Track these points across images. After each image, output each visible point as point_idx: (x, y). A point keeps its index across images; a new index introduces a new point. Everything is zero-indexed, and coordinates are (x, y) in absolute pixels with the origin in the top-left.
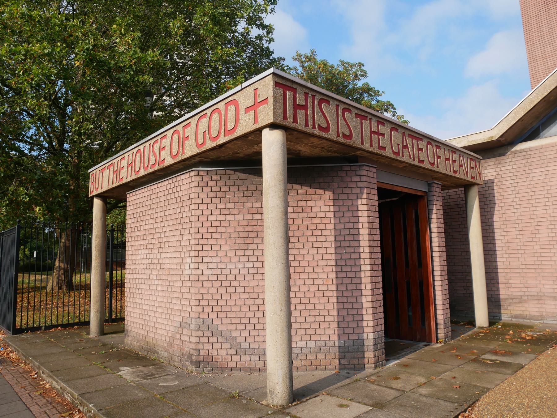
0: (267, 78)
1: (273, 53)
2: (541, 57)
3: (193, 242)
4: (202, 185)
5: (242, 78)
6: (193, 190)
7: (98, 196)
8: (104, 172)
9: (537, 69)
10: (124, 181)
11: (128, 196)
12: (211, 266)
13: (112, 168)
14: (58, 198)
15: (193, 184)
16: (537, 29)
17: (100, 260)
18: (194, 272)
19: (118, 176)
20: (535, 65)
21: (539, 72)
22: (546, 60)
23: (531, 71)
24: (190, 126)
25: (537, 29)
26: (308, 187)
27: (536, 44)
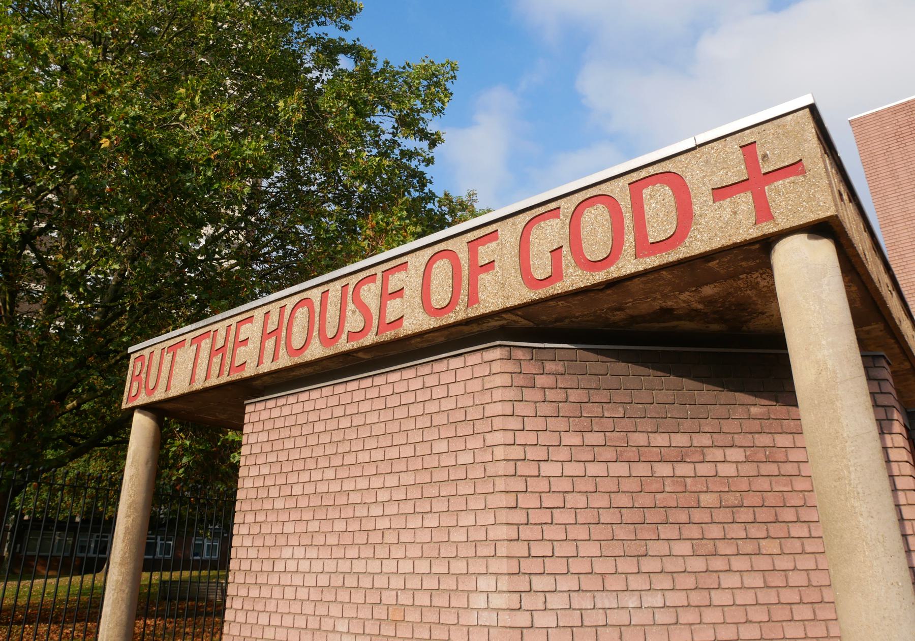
0: (789, 117)
1: (431, 183)
2: (902, 218)
3: (502, 532)
4: (521, 383)
5: (401, 210)
6: (498, 395)
7: (145, 408)
8: (179, 351)
9: (897, 236)
10: (249, 372)
11: (249, 409)
12: (556, 601)
13: (206, 344)
14: (8, 412)
15: (498, 380)
16: (889, 173)
17: (132, 566)
18: (506, 619)
19: (228, 361)
20: (893, 231)
21: (902, 242)
22: (910, 222)
23: (887, 239)
24: (496, 238)
25: (889, 173)
26: (770, 400)
27: (890, 196)
